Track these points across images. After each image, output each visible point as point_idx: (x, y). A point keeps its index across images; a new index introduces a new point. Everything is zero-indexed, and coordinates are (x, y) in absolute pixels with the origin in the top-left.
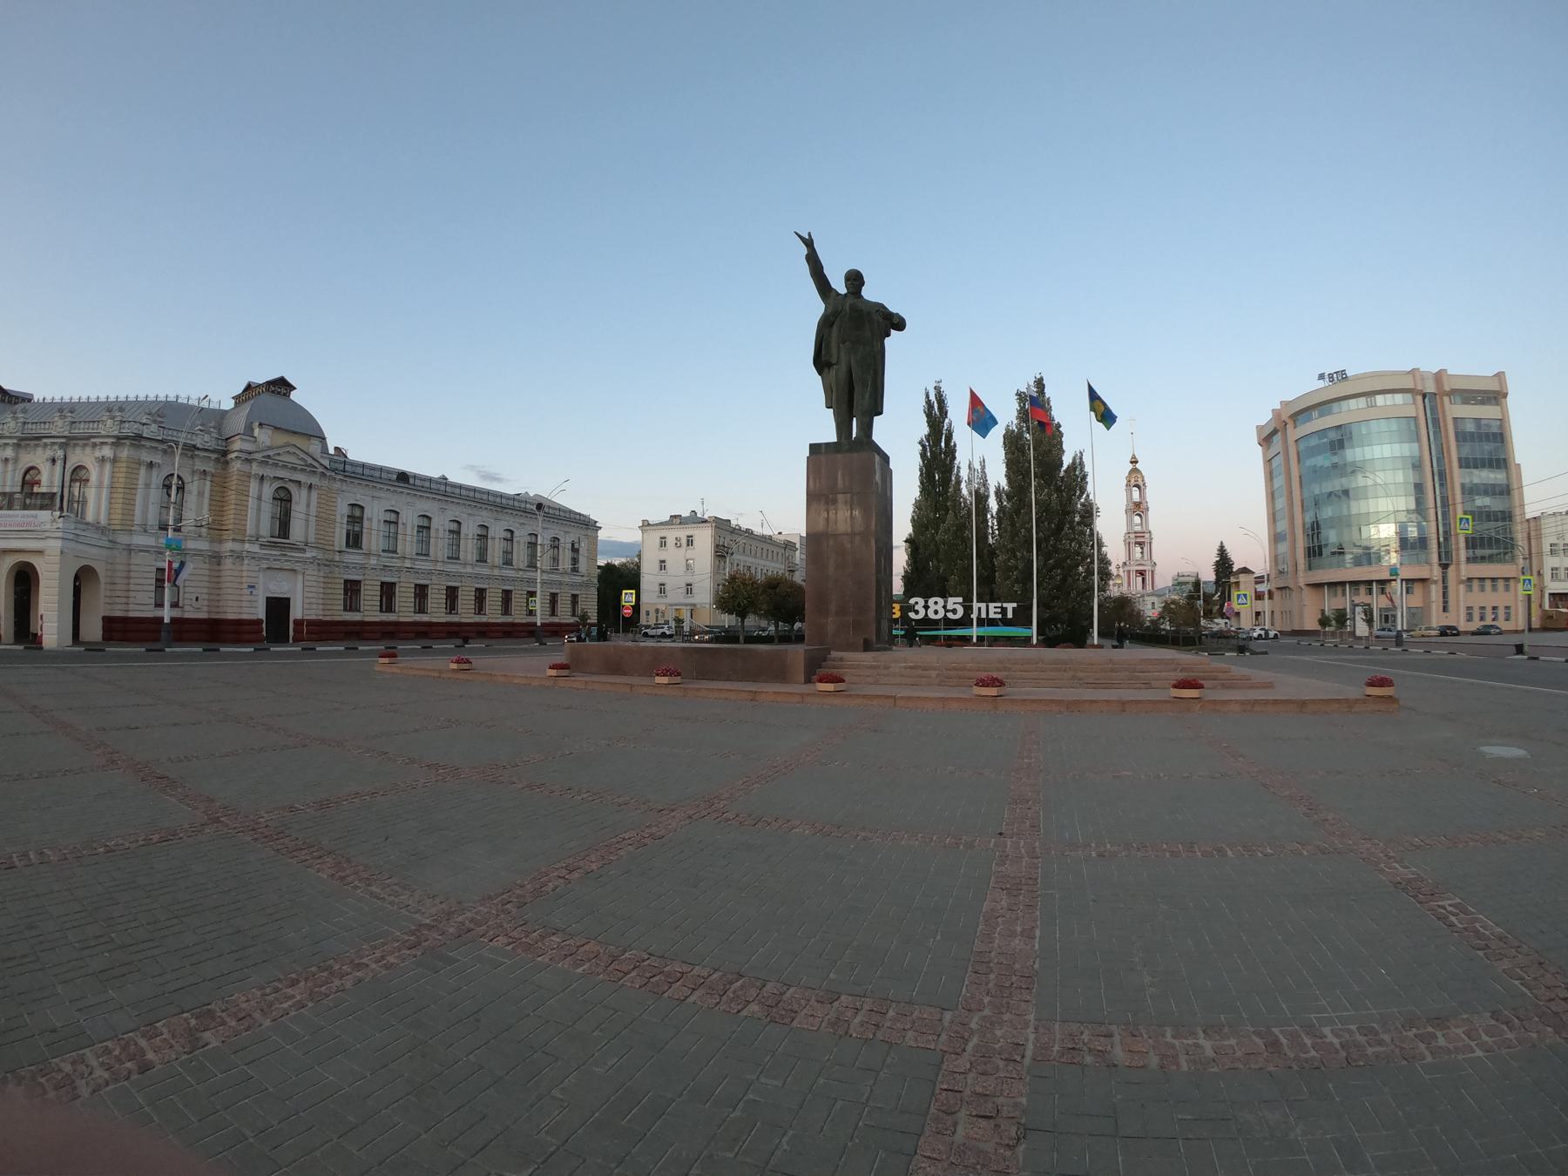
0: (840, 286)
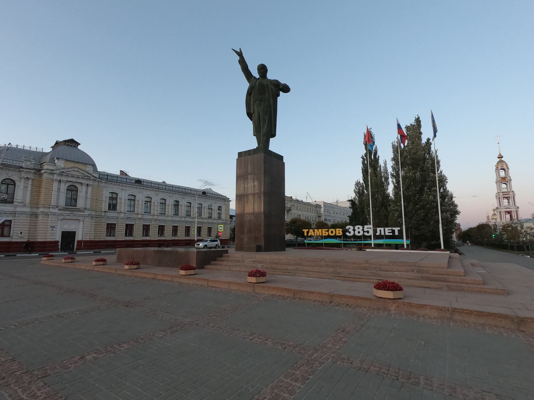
0: (255, 74)
